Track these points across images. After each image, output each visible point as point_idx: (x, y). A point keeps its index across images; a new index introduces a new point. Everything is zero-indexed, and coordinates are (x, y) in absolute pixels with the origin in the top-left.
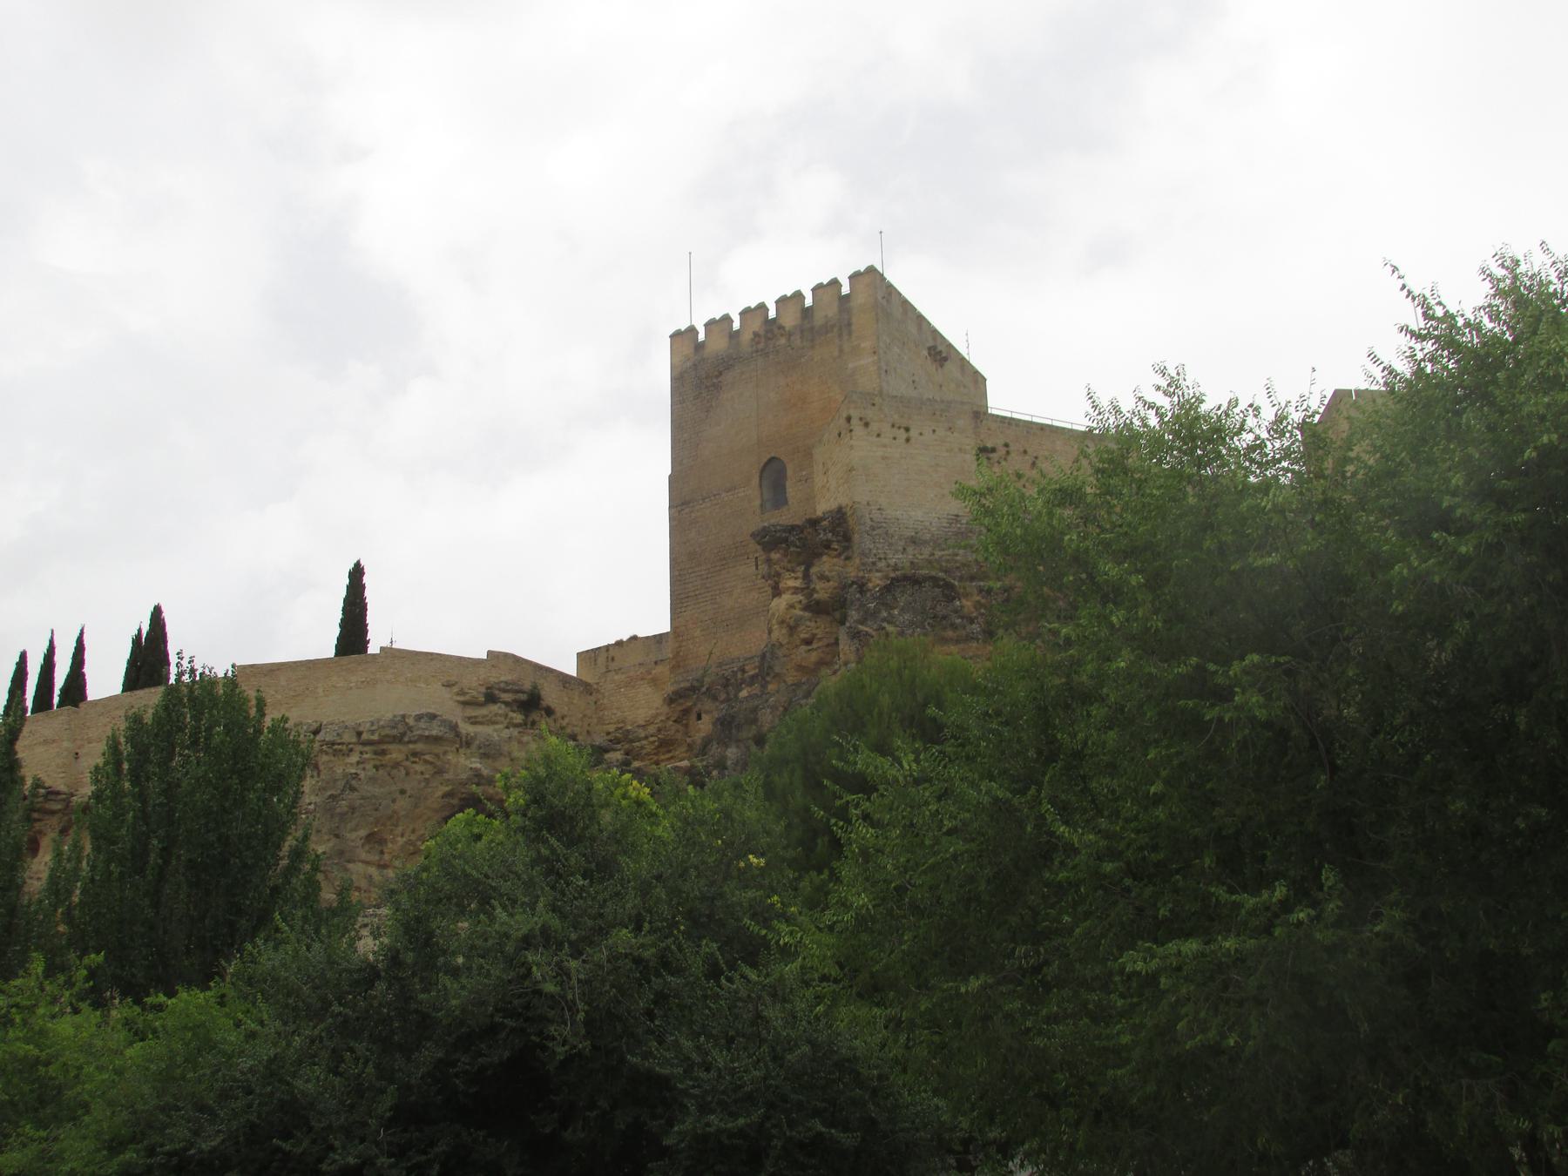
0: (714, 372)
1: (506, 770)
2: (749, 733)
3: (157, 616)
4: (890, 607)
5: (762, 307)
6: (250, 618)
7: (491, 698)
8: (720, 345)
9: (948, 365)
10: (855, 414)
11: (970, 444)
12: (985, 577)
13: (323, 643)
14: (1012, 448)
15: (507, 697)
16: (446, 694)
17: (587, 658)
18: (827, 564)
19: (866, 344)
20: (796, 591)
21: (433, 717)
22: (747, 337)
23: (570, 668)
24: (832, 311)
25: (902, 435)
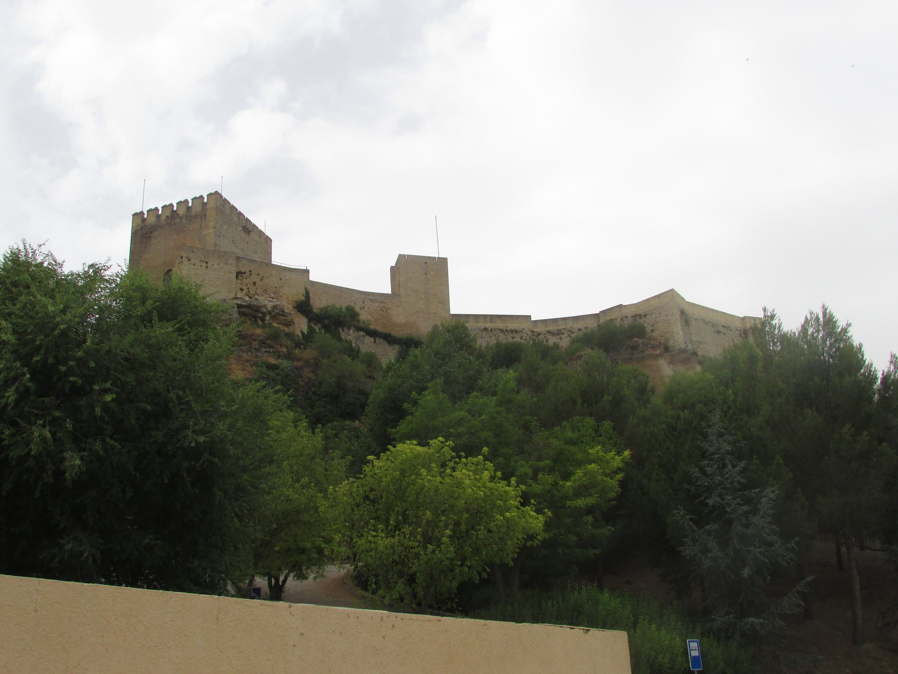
1: (847, 429)
3: (306, 289)
5: (171, 205)
8: (152, 220)
9: (252, 234)
10: (185, 255)
11: (234, 270)
14: (253, 272)
19: (211, 224)
22: (164, 217)
24: (198, 209)
25: (204, 265)
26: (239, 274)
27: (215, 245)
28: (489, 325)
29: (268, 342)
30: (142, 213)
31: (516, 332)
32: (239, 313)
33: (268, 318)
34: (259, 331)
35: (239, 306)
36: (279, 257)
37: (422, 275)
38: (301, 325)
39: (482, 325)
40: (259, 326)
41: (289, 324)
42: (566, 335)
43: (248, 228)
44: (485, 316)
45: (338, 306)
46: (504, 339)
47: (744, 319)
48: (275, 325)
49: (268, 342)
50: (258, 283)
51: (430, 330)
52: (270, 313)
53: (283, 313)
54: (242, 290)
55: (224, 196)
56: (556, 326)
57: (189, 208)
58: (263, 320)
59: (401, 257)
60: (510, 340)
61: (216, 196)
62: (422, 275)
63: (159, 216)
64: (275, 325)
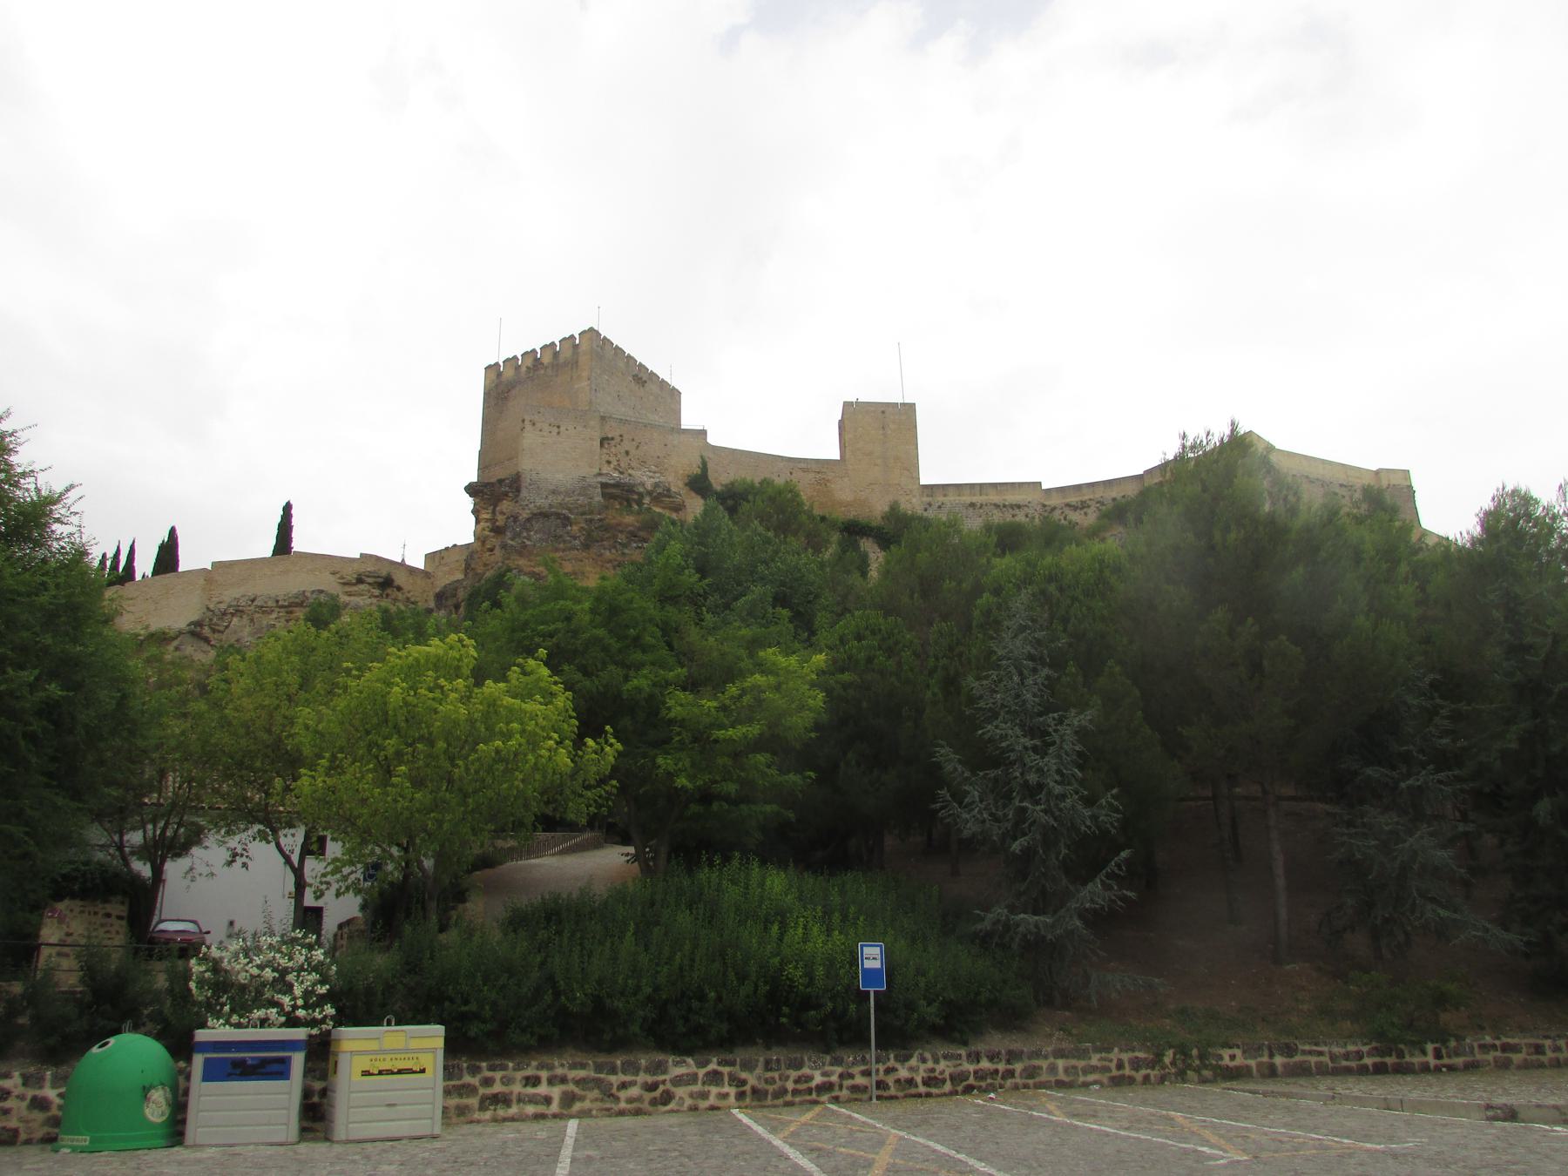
0: (512, 390)
2: (451, 602)
3: (173, 531)
4: (528, 530)
6: (1488, 504)
7: (360, 581)
8: (509, 374)
9: (649, 385)
10: (527, 418)
11: (597, 436)
12: (591, 513)
13: (264, 547)
15: (370, 580)
16: (332, 578)
17: (430, 557)
18: (505, 506)
19: (585, 374)
20: (487, 520)
21: (321, 592)
23: (418, 563)
24: (568, 354)
26: (604, 441)
27: (591, 402)
28: (977, 499)
29: (642, 534)
30: (497, 364)
31: (1019, 507)
32: (604, 495)
33: (647, 500)
34: (629, 519)
35: (604, 486)
36: (690, 419)
37: (881, 428)
38: (695, 507)
39: (967, 499)
40: (631, 512)
41: (678, 508)
42: (1093, 508)
43: (642, 377)
44: (972, 486)
45: (749, 479)
46: (997, 518)
47: (1378, 473)
48: (658, 510)
49: (642, 534)
50: (633, 452)
51: (887, 509)
52: (649, 493)
53: (668, 493)
54: (609, 462)
55: (603, 334)
56: (1078, 496)
57: (556, 354)
58: (639, 503)
59: (847, 405)
60: (1009, 518)
61: (591, 333)
62: (881, 428)
63: (518, 368)
64: (658, 510)
